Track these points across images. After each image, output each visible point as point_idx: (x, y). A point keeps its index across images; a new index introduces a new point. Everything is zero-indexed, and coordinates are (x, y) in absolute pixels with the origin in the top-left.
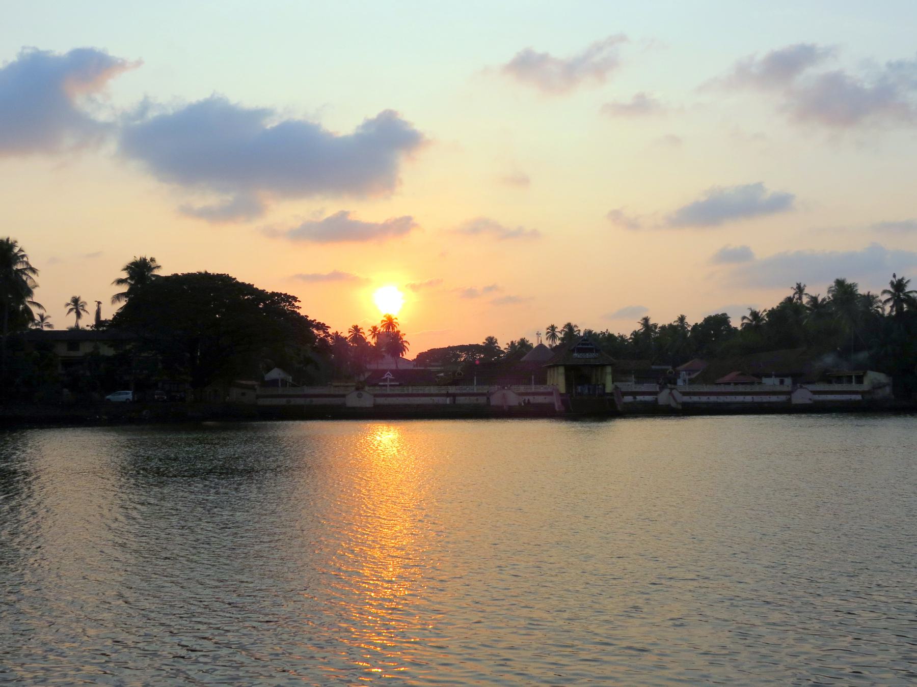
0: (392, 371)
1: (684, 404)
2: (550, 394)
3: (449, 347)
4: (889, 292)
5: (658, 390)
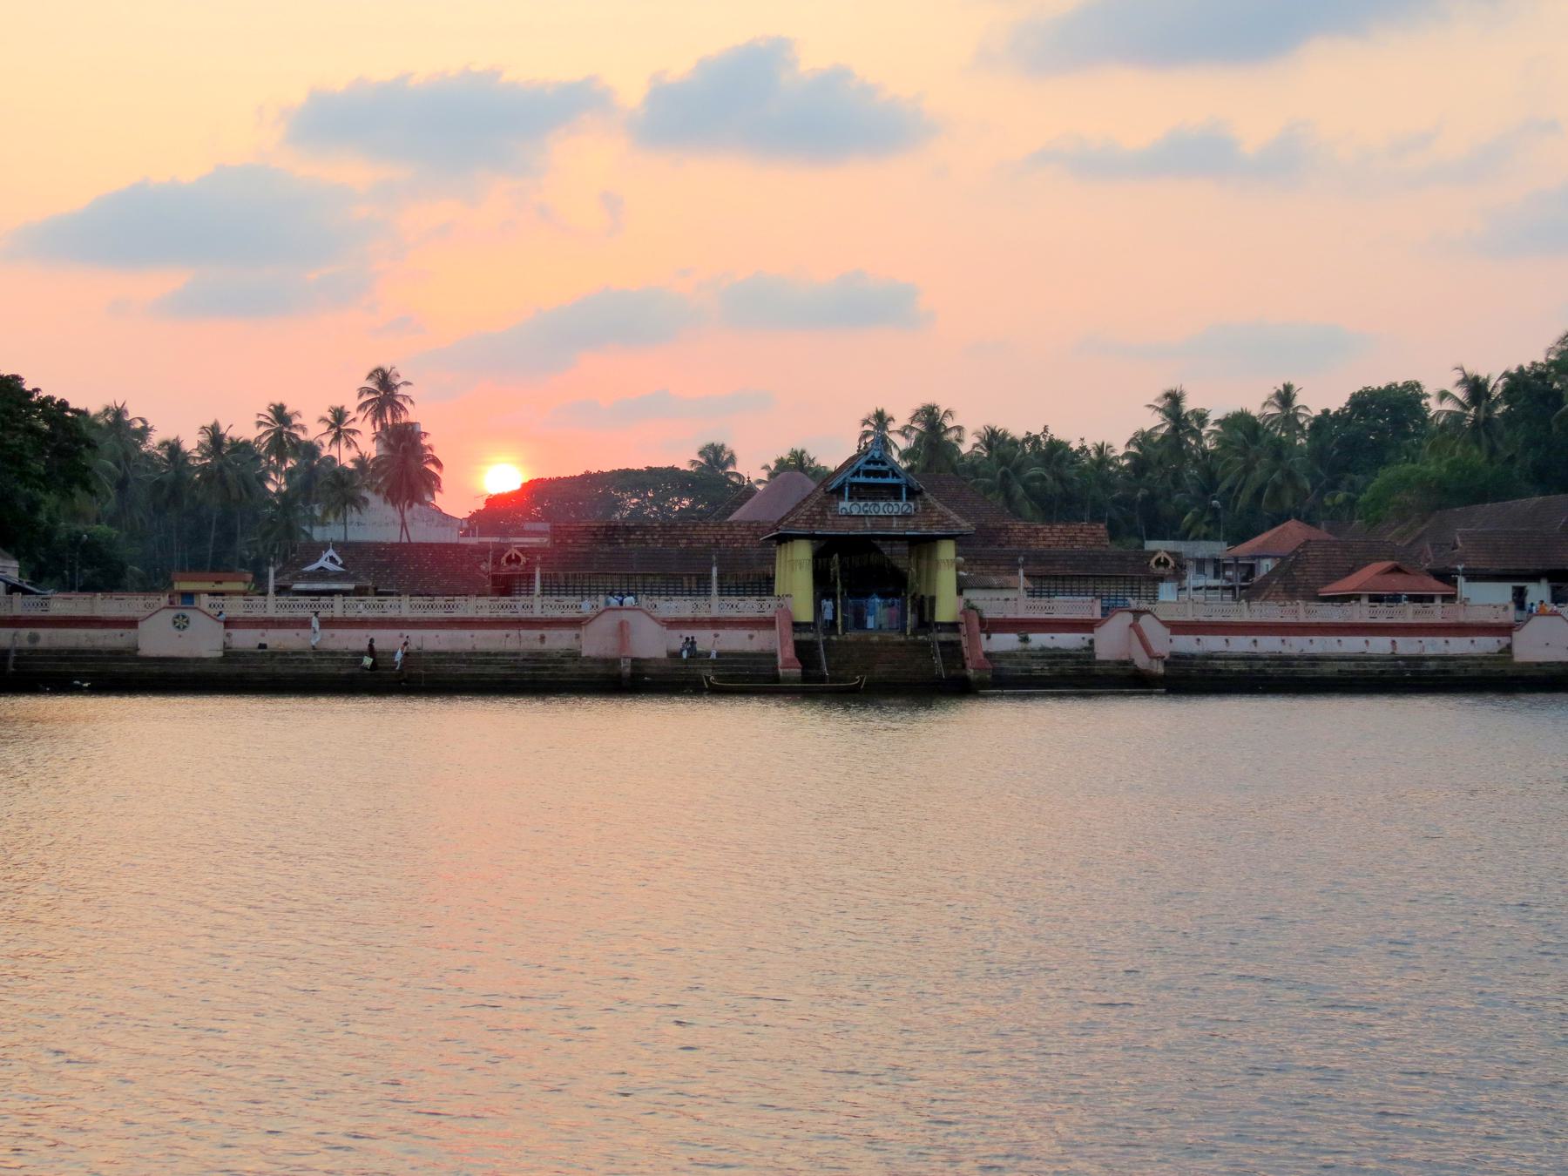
0: (337, 546)
1: (1176, 659)
2: (769, 623)
3: (587, 476)
4: (370, 391)
5: (1098, 615)
